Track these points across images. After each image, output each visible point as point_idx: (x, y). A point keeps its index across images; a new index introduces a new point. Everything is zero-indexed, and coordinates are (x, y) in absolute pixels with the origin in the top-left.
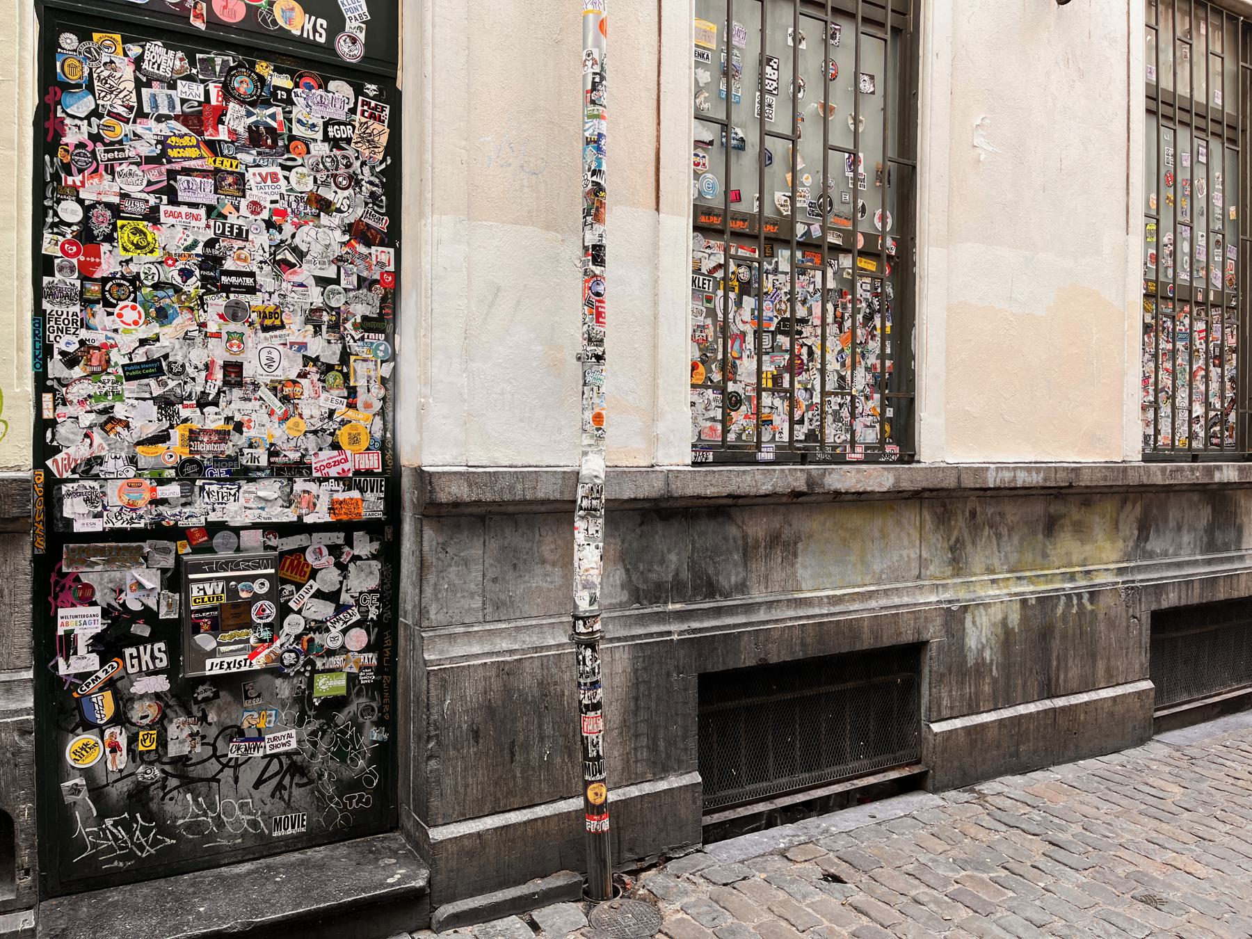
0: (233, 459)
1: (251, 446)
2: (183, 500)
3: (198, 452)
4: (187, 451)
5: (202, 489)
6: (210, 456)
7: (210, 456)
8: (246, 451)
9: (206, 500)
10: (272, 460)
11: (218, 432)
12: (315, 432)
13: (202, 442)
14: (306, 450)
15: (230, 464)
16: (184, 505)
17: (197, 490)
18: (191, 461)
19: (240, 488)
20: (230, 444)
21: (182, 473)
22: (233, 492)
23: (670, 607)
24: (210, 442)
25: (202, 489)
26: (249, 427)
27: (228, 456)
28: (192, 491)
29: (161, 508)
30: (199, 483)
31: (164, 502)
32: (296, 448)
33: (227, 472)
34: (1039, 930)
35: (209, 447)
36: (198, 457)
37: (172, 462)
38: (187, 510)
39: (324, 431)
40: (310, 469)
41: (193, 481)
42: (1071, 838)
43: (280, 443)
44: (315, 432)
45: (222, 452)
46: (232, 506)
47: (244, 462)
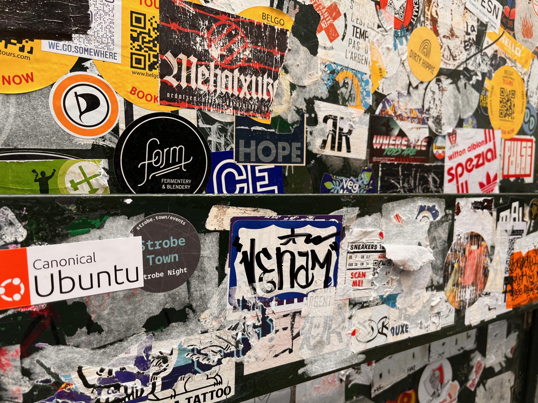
0: (289, 133)
1: (334, 96)
2: (156, 302)
3: (190, 97)
4: (152, 84)
5: (228, 242)
6: (227, 116)
7: (227, 116)
8: (323, 109)
9: (243, 290)
10: (379, 141)
11: (253, 30)
12: (453, 75)
13: (203, 58)
14: (438, 120)
15: (283, 148)
16: (157, 324)
17: (209, 249)
18: (164, 130)
19: (340, 235)
20: (285, 80)
21: (135, 175)
22: (321, 250)
23: (182, 195)
24: (227, 64)
25: (228, 242)
26: (332, 35)
27: (278, 121)
28: (191, 259)
29: (51, 356)
30: (218, 219)
31: (66, 320)
32: (421, 117)
33: (276, 176)
34: (358, 343)
35: (227, 82)
36: (189, 115)
37: (99, 125)
38: (171, 345)
39: (468, 74)
40: (439, 171)
41: (197, 213)
42: (501, 343)
43: (393, 96)
44: (453, 75)
45: (264, 106)
46: (320, 304)
47: (316, 146)
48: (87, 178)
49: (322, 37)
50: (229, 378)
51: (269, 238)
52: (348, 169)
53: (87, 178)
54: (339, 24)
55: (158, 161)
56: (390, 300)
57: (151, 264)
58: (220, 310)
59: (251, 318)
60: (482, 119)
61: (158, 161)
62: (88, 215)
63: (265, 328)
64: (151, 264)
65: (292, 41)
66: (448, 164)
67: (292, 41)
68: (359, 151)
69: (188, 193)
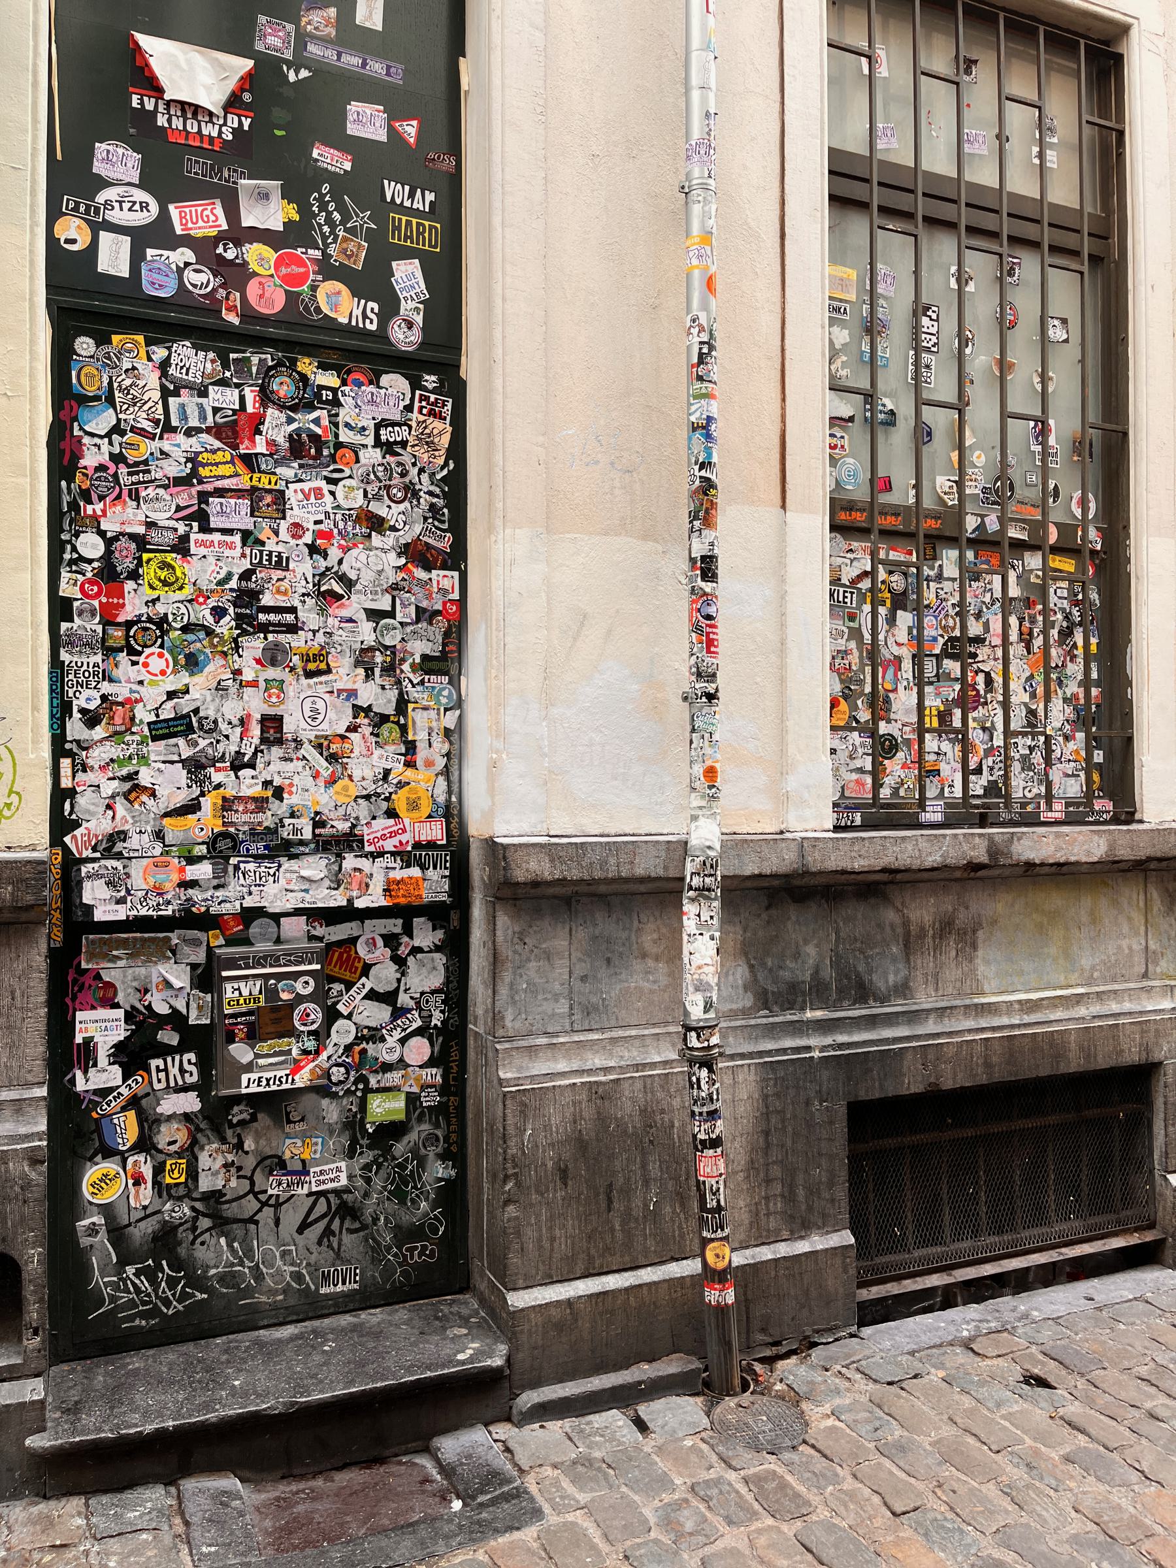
0: (272, 832)
1: (292, 815)
3: (232, 824)
5: (237, 868)
6: (246, 828)
7: (246, 828)
8: (287, 821)
9: (242, 881)
10: (317, 831)
12: (367, 797)
13: (237, 811)
14: (357, 818)
15: (269, 837)
16: (216, 887)
17: (231, 869)
18: (224, 835)
19: (280, 866)
20: (269, 813)
21: (215, 849)
22: (272, 871)
24: (245, 812)
25: (237, 868)
28: (225, 871)
29: (190, 891)
32: (346, 817)
35: (245, 818)
36: (232, 830)
38: (220, 893)
43: (326, 811)
44: (367, 797)
45: (260, 824)
47: (285, 835)
48: (202, 850)
49: (285, 795)
50: (238, 907)
51: (251, 866)
52: (302, 843)
53: (202, 850)
54: (294, 789)
55: (222, 845)
56: (306, 891)
57: (224, 974)
58: (235, 887)
59: (245, 890)
60: (391, 814)
61: (222, 845)
62: (200, 859)
63: (250, 893)
64: (224, 974)
65: (271, 799)
66: (366, 838)
67: (271, 799)
68: (307, 834)
69: (867, 1029)
